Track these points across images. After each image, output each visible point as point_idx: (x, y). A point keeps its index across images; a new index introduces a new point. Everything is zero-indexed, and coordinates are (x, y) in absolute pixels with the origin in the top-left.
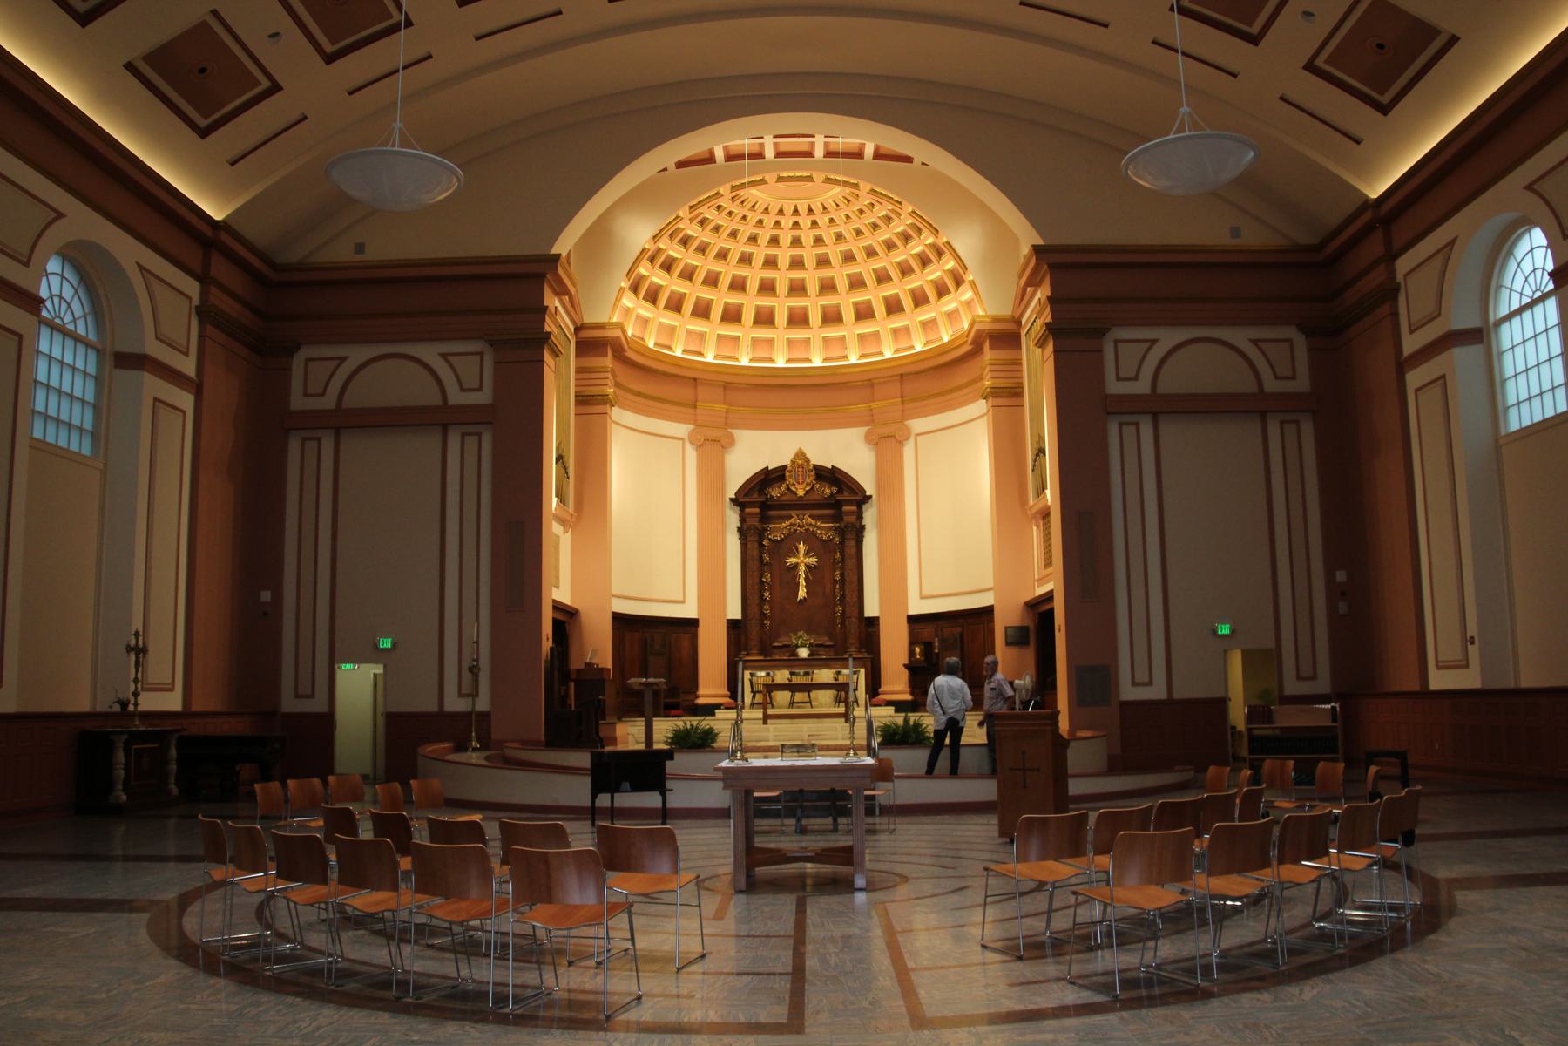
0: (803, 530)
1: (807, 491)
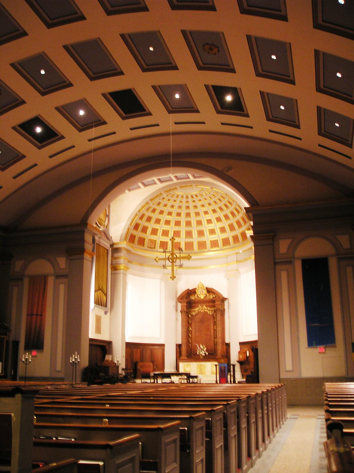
0: (203, 311)
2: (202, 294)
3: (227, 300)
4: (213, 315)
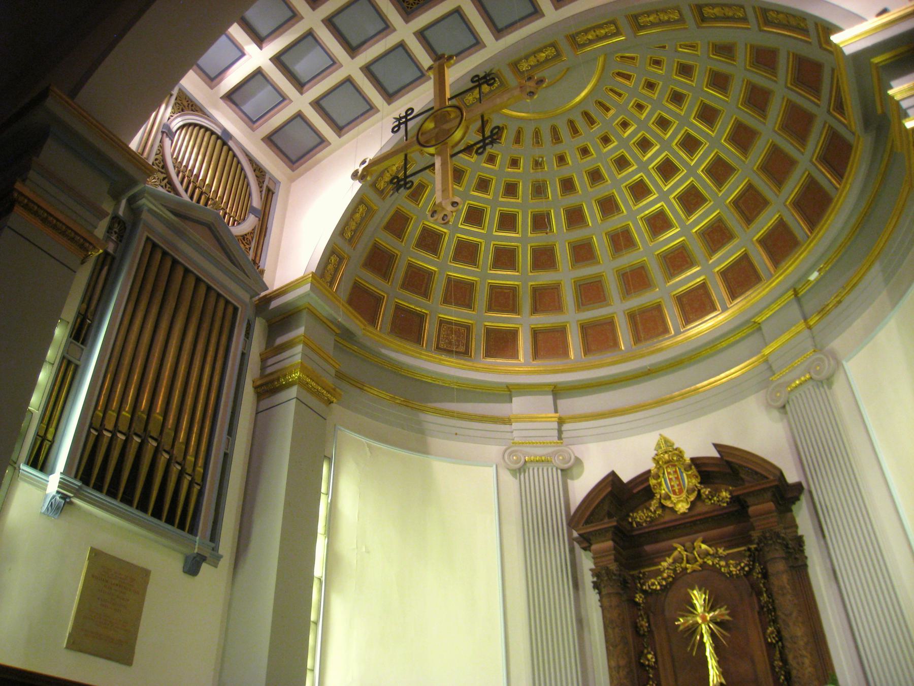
0: (696, 566)
1: (692, 502)
2: (681, 491)
3: (804, 498)
4: (748, 574)
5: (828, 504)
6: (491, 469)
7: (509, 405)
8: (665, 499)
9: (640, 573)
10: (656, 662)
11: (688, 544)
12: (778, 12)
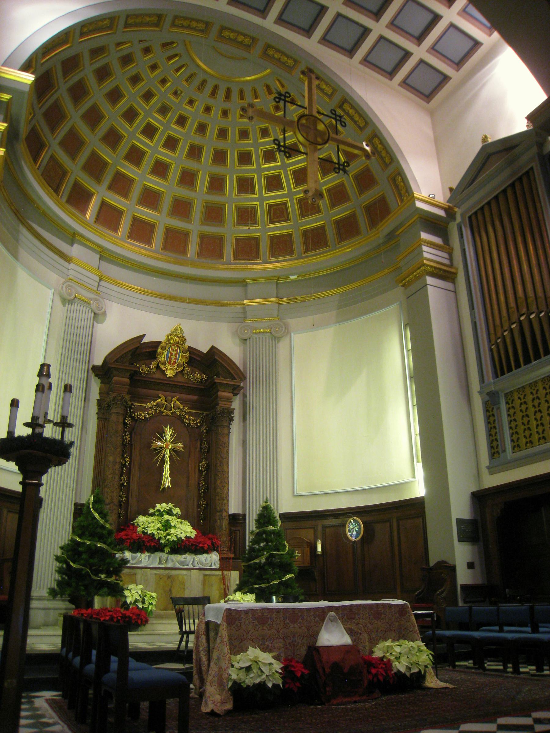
0: (169, 413)
2: (174, 363)
4: (199, 427)
5: (254, 406)
6: (51, 291)
7: (70, 247)
8: (162, 364)
9: (132, 404)
10: (130, 464)
11: (169, 398)
12: (381, 143)
